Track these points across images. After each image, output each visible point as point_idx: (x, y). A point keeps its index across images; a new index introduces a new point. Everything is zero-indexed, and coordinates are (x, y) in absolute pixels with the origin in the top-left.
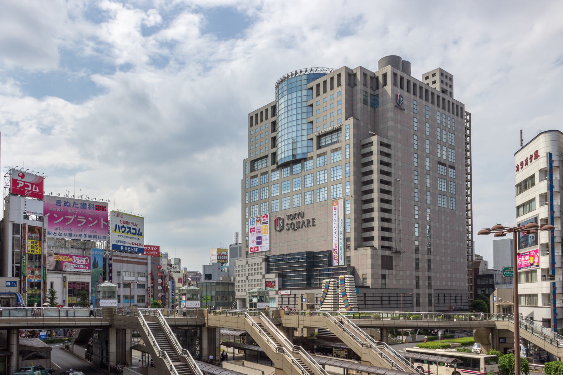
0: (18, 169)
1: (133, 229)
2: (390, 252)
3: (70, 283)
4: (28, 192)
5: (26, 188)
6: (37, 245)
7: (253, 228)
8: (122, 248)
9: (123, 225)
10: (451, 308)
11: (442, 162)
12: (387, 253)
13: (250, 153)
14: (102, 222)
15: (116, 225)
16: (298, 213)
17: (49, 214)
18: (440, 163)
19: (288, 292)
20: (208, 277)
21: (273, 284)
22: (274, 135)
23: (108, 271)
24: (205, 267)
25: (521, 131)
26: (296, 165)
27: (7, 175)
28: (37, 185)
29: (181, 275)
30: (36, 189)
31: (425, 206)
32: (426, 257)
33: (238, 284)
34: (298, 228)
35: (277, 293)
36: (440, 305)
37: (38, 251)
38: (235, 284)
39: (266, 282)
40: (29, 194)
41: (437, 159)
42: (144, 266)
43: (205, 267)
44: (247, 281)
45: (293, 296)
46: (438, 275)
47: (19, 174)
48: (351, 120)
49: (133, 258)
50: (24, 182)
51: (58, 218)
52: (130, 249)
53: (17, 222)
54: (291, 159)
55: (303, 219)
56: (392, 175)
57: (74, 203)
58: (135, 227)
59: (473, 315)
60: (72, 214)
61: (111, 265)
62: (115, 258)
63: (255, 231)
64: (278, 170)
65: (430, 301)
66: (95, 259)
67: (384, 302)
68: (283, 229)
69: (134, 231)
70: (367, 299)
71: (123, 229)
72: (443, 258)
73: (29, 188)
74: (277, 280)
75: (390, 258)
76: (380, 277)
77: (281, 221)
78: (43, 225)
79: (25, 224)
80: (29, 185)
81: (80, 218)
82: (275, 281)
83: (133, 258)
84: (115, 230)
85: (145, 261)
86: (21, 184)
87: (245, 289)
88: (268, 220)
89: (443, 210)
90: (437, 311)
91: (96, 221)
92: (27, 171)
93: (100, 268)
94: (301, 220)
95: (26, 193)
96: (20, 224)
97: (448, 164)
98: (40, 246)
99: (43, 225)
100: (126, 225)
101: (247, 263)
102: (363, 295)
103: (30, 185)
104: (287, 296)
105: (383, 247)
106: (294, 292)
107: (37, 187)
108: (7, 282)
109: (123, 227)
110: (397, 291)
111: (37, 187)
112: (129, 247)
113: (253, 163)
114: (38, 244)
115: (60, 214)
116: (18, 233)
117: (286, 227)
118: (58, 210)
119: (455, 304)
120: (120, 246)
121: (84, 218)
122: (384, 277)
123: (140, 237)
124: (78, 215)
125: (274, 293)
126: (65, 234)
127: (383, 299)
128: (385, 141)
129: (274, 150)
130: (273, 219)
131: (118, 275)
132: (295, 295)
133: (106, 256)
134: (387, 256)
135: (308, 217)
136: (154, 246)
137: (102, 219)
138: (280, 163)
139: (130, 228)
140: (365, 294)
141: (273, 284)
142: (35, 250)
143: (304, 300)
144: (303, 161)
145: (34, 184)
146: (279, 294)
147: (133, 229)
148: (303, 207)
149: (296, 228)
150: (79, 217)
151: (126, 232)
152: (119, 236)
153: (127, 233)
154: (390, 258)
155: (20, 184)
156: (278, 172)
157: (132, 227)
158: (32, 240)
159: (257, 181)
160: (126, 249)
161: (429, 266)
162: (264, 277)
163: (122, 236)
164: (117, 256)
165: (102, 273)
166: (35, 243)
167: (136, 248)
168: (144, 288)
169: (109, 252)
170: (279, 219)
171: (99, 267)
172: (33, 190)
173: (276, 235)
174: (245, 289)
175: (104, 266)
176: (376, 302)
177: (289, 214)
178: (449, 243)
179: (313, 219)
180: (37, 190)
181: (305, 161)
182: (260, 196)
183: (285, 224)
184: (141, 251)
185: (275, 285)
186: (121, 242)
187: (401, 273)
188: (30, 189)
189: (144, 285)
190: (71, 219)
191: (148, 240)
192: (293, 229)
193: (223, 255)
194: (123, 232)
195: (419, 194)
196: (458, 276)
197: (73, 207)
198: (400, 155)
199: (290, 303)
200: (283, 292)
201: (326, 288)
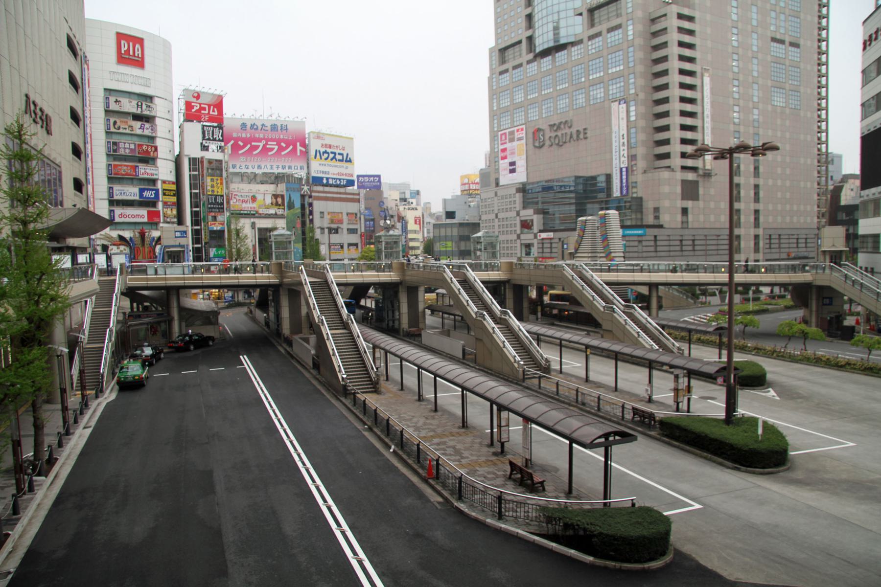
0: (192, 88)
1: (339, 154)
2: (695, 175)
3: (260, 230)
8: (325, 181)
10: (789, 256)
11: (778, 37)
12: (690, 176)
13: (497, 39)
14: (299, 148)
15: (316, 151)
16: (564, 121)
17: (232, 142)
18: (774, 40)
19: (551, 235)
20: (450, 215)
22: (529, 11)
24: (445, 201)
27: (181, 97)
29: (418, 213)
30: (214, 111)
31: (751, 105)
32: (752, 181)
33: (485, 225)
34: (565, 142)
35: (535, 237)
36: (773, 250)
37: (219, 190)
38: (481, 225)
41: (769, 35)
43: (445, 201)
44: (496, 220)
46: (770, 207)
49: (340, 193)
50: (200, 104)
51: (244, 146)
53: (193, 156)
54: (551, 44)
55: (571, 130)
56: (698, 61)
57: (263, 125)
58: (341, 152)
59: (303, 264)
60: (260, 140)
61: (311, 205)
64: (535, 60)
65: (756, 244)
67: (684, 248)
68: (543, 145)
69: (339, 157)
70: (658, 243)
71: (326, 155)
72: (779, 183)
75: (695, 184)
76: (680, 211)
77: (541, 133)
79: (202, 158)
81: (273, 145)
83: (340, 193)
84: (315, 158)
85: (357, 197)
87: (515, 231)
88: (524, 135)
89: (779, 110)
90: (767, 260)
91: (291, 147)
92: (203, 90)
94: (568, 131)
97: (787, 40)
100: (329, 150)
101: (496, 194)
102: (653, 238)
104: (548, 241)
105: (684, 168)
107: (215, 109)
108: (176, 232)
109: (326, 152)
110: (706, 232)
111: (215, 109)
113: (503, 52)
114: (219, 182)
115: (246, 141)
116: (195, 170)
117: (548, 143)
118: (244, 135)
119: (796, 250)
120: (322, 178)
122: (685, 211)
123: (348, 164)
124: (268, 140)
125: (531, 236)
127: (684, 243)
128: (686, 12)
129: (529, 33)
130: (531, 130)
131: (321, 217)
134: (691, 181)
135: (578, 126)
136: (374, 176)
137: (298, 144)
138: (538, 50)
139: (335, 153)
140: (655, 237)
144: (569, 47)
147: (339, 154)
148: (571, 113)
149: (561, 144)
150: (269, 143)
151: (330, 158)
153: (332, 159)
154: (695, 184)
156: (536, 63)
157: (337, 151)
160: (331, 182)
161: (757, 194)
162: (518, 214)
164: (319, 192)
165: (300, 216)
168: (357, 233)
170: (539, 130)
171: (296, 207)
175: (303, 207)
176: (672, 248)
177: (552, 123)
178: (788, 159)
179: (585, 129)
182: (512, 100)
183: (547, 137)
184: (351, 183)
186: (323, 172)
187: (712, 205)
188: (207, 112)
189: (357, 229)
190: (259, 146)
191: (361, 167)
192: (558, 144)
194: (326, 159)
195: (741, 88)
196: (802, 208)
198: (709, 31)
200: (544, 235)
201: (581, 229)
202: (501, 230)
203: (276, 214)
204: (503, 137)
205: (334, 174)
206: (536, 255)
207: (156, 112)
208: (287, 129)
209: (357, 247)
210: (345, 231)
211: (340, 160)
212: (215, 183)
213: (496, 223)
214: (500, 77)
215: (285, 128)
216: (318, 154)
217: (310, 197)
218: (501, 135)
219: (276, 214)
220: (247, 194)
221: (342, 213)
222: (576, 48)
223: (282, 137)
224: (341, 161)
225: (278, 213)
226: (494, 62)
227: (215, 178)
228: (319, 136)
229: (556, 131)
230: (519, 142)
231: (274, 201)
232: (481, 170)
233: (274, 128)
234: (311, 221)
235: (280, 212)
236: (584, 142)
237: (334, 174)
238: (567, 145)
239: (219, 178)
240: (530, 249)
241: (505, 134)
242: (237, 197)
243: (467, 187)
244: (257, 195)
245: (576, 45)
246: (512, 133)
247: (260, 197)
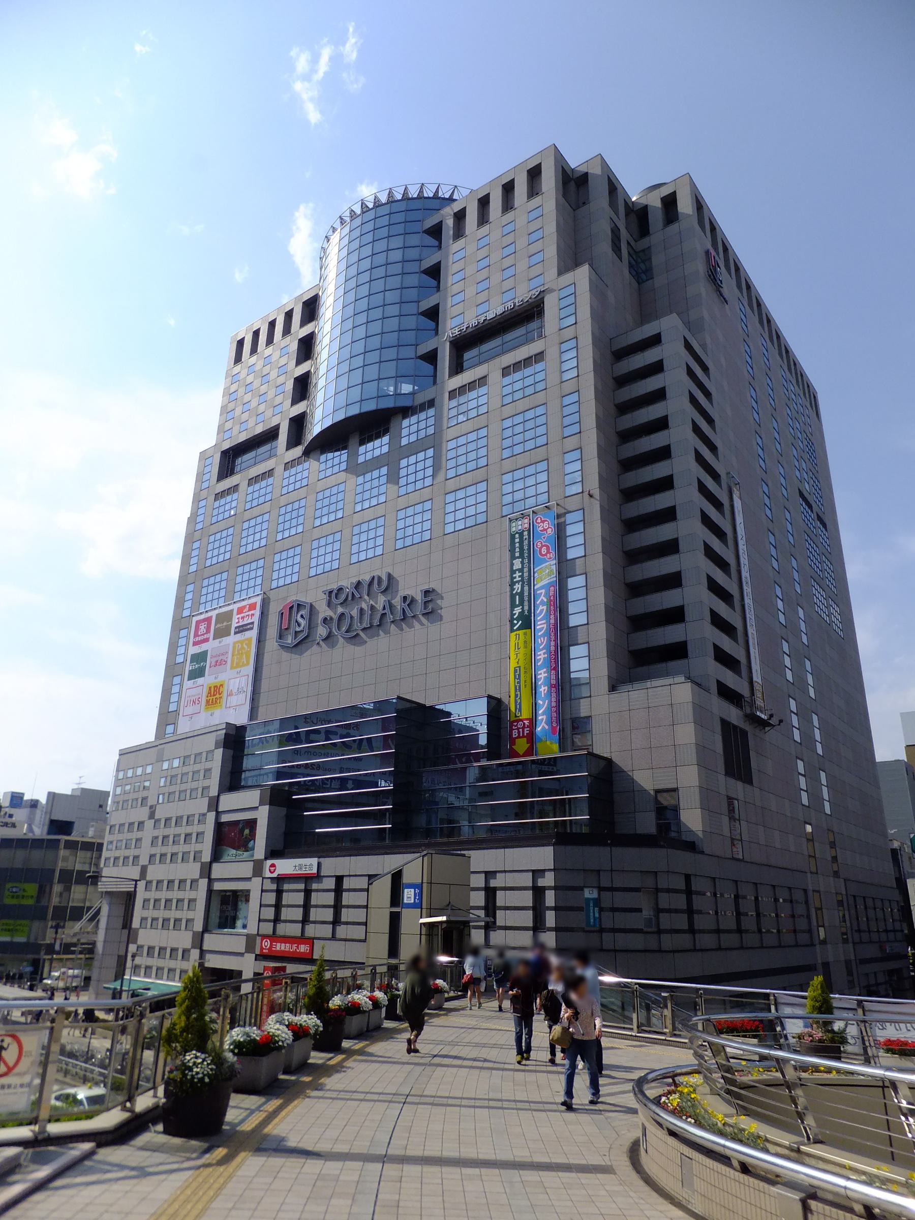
19: (308, 865)
21: (247, 831)
33: (116, 837)
36: (668, 941)
39: (219, 826)
45: (330, 883)
48: (583, 272)
74: (262, 815)
87: (136, 858)
106: (334, 865)
117: (322, 631)
125: (246, 869)
132: (339, 879)
141: (247, 831)
143: (409, 895)
146: (268, 874)
173: (279, 662)
174: (136, 858)
179: (427, 593)
181: (404, 418)
185: (253, 836)
199: (285, 914)
200: (286, 866)
202: (158, 850)
204: (203, 628)
206: (252, 929)
213: (149, 831)
214: (217, 504)
218: (198, 623)
222: (414, 419)
230: (239, 637)
240: (236, 908)
241: (208, 620)
246: (228, 616)
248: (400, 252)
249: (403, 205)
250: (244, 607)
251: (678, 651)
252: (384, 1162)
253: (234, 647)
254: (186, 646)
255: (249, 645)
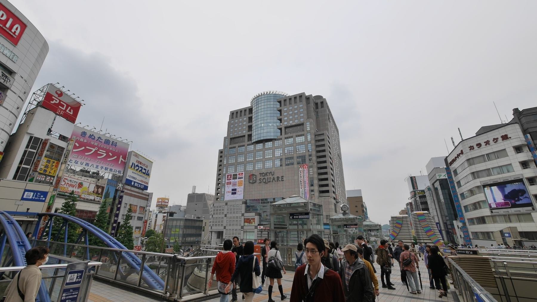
0: (58, 86)
1: (145, 169)
4: (61, 111)
5: (60, 107)
6: (53, 166)
7: (229, 182)
8: (133, 184)
9: (138, 165)
14: (121, 159)
15: (133, 163)
23: (117, 202)
25: (459, 128)
26: (268, 143)
28: (72, 108)
30: (70, 111)
34: (270, 182)
37: (52, 172)
40: (61, 113)
42: (146, 201)
47: (57, 92)
49: (139, 193)
50: (60, 101)
52: (138, 185)
55: (274, 176)
58: (145, 168)
60: (94, 147)
61: (121, 197)
62: (126, 191)
63: (231, 184)
64: (253, 145)
66: (108, 190)
68: (255, 182)
69: (143, 171)
71: (137, 168)
73: (63, 107)
78: (68, 146)
79: (47, 140)
80: (64, 105)
81: (101, 152)
82: (254, 219)
84: (131, 167)
85: (147, 197)
86: (56, 101)
88: (243, 176)
92: (67, 92)
93: (110, 199)
95: (59, 111)
96: (40, 139)
98: (57, 166)
99: (68, 146)
100: (140, 165)
103: (65, 106)
107: (72, 110)
108: (26, 190)
109: (137, 166)
111: (72, 110)
112: (138, 183)
114: (54, 164)
117: (258, 181)
118: (82, 140)
120: (132, 181)
121: (105, 152)
124: (100, 148)
126: (82, 163)
129: (250, 133)
130: (248, 175)
133: (119, 188)
137: (121, 156)
142: (49, 170)
143: (507, 235)
145: (70, 106)
146: (259, 228)
147: (145, 169)
149: (267, 182)
150: (100, 150)
151: (139, 170)
152: (133, 172)
153: (140, 171)
155: (54, 101)
156: (253, 146)
157: (144, 167)
158: (49, 159)
159: (235, 151)
160: (136, 185)
163: (135, 174)
166: (51, 163)
167: (143, 185)
169: (122, 185)
170: (253, 175)
172: (67, 111)
179: (278, 177)
180: (71, 112)
186: (133, 178)
188: (64, 109)
190: (92, 150)
193: (166, 202)
197: (97, 140)
203: (94, 200)
204: (229, 177)
205: (139, 180)
207: (3, 104)
208: (116, 145)
209: (140, 230)
210: (136, 218)
211: (144, 173)
212: (50, 165)
215: (114, 144)
216: (133, 166)
217: (123, 192)
219: (94, 200)
220: (76, 180)
221: (137, 206)
222: (277, 141)
223: (111, 149)
224: (144, 173)
225: (96, 200)
226: (227, 143)
227: (52, 161)
228: (137, 155)
229: (264, 176)
230: (239, 180)
231: (96, 190)
232: (189, 194)
233: (107, 142)
234: (119, 209)
235: (98, 199)
236: (281, 182)
237: (139, 180)
238: (271, 183)
239: (56, 162)
242: (67, 181)
243: (160, 203)
244: (84, 183)
245: (277, 140)
247: (86, 185)
248: (271, 104)
249: (266, 96)
250: (240, 174)
251: (328, 191)
252: (177, 221)
253: (238, 182)
254: (225, 180)
255: (242, 182)
